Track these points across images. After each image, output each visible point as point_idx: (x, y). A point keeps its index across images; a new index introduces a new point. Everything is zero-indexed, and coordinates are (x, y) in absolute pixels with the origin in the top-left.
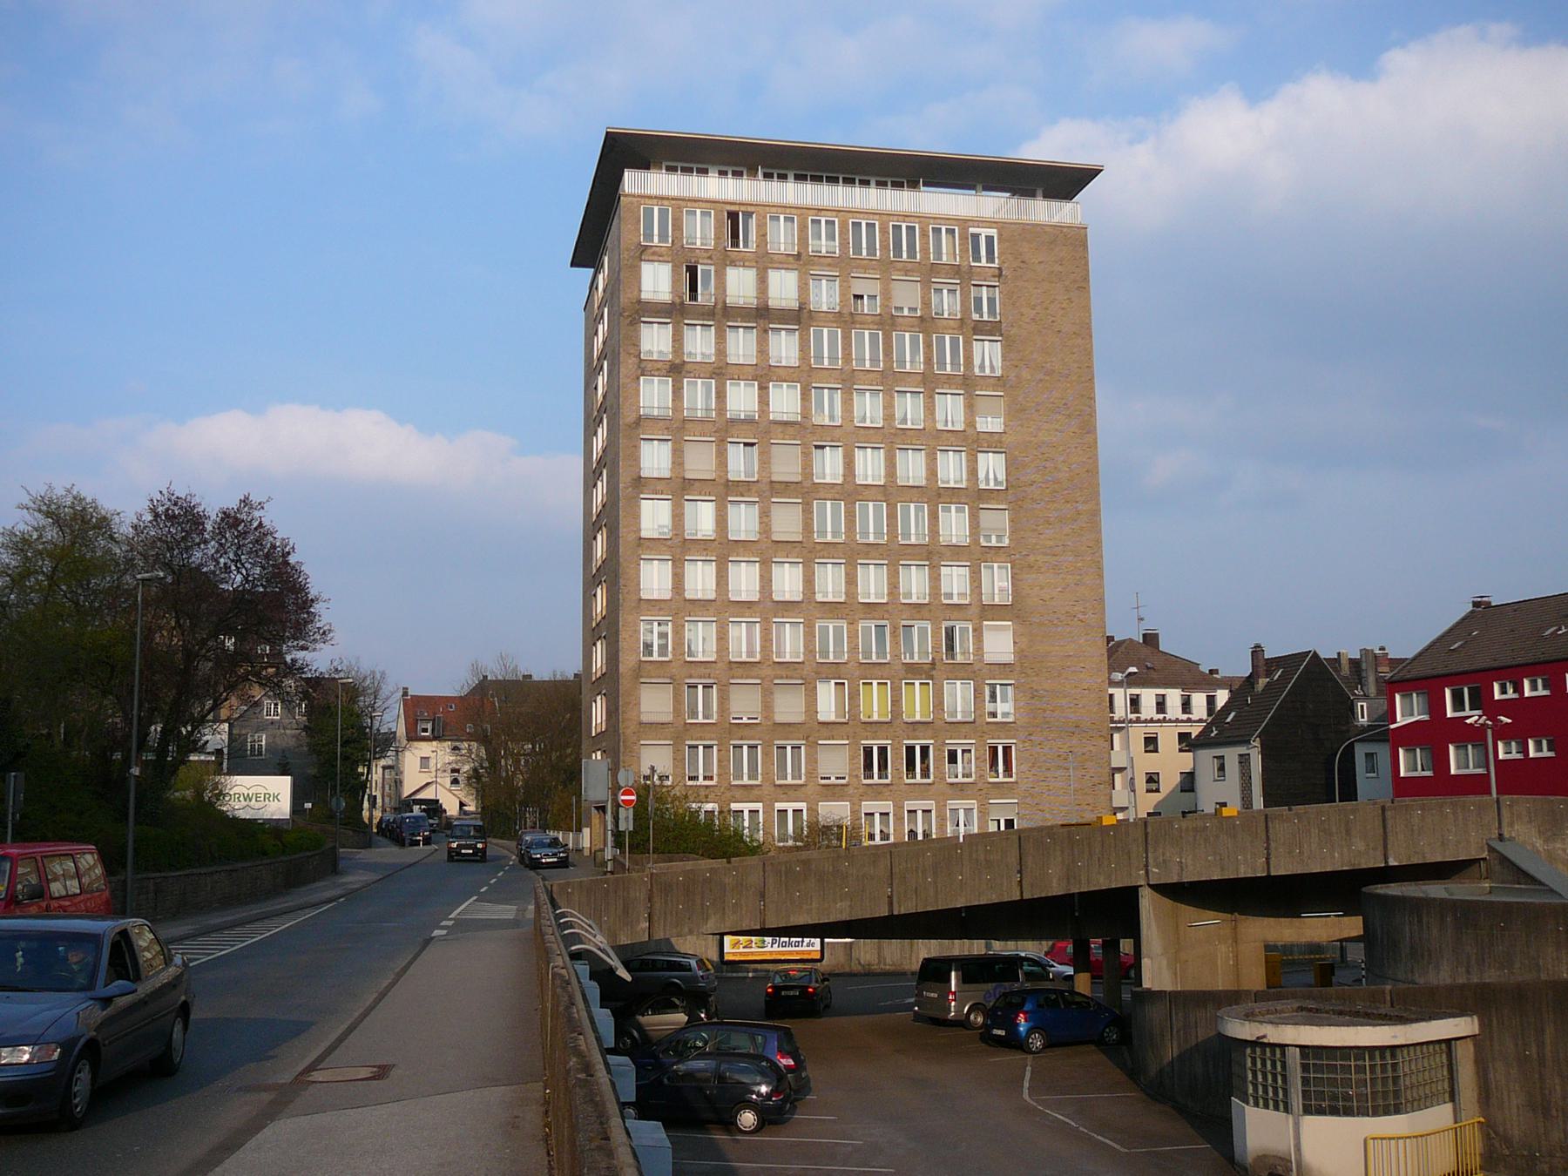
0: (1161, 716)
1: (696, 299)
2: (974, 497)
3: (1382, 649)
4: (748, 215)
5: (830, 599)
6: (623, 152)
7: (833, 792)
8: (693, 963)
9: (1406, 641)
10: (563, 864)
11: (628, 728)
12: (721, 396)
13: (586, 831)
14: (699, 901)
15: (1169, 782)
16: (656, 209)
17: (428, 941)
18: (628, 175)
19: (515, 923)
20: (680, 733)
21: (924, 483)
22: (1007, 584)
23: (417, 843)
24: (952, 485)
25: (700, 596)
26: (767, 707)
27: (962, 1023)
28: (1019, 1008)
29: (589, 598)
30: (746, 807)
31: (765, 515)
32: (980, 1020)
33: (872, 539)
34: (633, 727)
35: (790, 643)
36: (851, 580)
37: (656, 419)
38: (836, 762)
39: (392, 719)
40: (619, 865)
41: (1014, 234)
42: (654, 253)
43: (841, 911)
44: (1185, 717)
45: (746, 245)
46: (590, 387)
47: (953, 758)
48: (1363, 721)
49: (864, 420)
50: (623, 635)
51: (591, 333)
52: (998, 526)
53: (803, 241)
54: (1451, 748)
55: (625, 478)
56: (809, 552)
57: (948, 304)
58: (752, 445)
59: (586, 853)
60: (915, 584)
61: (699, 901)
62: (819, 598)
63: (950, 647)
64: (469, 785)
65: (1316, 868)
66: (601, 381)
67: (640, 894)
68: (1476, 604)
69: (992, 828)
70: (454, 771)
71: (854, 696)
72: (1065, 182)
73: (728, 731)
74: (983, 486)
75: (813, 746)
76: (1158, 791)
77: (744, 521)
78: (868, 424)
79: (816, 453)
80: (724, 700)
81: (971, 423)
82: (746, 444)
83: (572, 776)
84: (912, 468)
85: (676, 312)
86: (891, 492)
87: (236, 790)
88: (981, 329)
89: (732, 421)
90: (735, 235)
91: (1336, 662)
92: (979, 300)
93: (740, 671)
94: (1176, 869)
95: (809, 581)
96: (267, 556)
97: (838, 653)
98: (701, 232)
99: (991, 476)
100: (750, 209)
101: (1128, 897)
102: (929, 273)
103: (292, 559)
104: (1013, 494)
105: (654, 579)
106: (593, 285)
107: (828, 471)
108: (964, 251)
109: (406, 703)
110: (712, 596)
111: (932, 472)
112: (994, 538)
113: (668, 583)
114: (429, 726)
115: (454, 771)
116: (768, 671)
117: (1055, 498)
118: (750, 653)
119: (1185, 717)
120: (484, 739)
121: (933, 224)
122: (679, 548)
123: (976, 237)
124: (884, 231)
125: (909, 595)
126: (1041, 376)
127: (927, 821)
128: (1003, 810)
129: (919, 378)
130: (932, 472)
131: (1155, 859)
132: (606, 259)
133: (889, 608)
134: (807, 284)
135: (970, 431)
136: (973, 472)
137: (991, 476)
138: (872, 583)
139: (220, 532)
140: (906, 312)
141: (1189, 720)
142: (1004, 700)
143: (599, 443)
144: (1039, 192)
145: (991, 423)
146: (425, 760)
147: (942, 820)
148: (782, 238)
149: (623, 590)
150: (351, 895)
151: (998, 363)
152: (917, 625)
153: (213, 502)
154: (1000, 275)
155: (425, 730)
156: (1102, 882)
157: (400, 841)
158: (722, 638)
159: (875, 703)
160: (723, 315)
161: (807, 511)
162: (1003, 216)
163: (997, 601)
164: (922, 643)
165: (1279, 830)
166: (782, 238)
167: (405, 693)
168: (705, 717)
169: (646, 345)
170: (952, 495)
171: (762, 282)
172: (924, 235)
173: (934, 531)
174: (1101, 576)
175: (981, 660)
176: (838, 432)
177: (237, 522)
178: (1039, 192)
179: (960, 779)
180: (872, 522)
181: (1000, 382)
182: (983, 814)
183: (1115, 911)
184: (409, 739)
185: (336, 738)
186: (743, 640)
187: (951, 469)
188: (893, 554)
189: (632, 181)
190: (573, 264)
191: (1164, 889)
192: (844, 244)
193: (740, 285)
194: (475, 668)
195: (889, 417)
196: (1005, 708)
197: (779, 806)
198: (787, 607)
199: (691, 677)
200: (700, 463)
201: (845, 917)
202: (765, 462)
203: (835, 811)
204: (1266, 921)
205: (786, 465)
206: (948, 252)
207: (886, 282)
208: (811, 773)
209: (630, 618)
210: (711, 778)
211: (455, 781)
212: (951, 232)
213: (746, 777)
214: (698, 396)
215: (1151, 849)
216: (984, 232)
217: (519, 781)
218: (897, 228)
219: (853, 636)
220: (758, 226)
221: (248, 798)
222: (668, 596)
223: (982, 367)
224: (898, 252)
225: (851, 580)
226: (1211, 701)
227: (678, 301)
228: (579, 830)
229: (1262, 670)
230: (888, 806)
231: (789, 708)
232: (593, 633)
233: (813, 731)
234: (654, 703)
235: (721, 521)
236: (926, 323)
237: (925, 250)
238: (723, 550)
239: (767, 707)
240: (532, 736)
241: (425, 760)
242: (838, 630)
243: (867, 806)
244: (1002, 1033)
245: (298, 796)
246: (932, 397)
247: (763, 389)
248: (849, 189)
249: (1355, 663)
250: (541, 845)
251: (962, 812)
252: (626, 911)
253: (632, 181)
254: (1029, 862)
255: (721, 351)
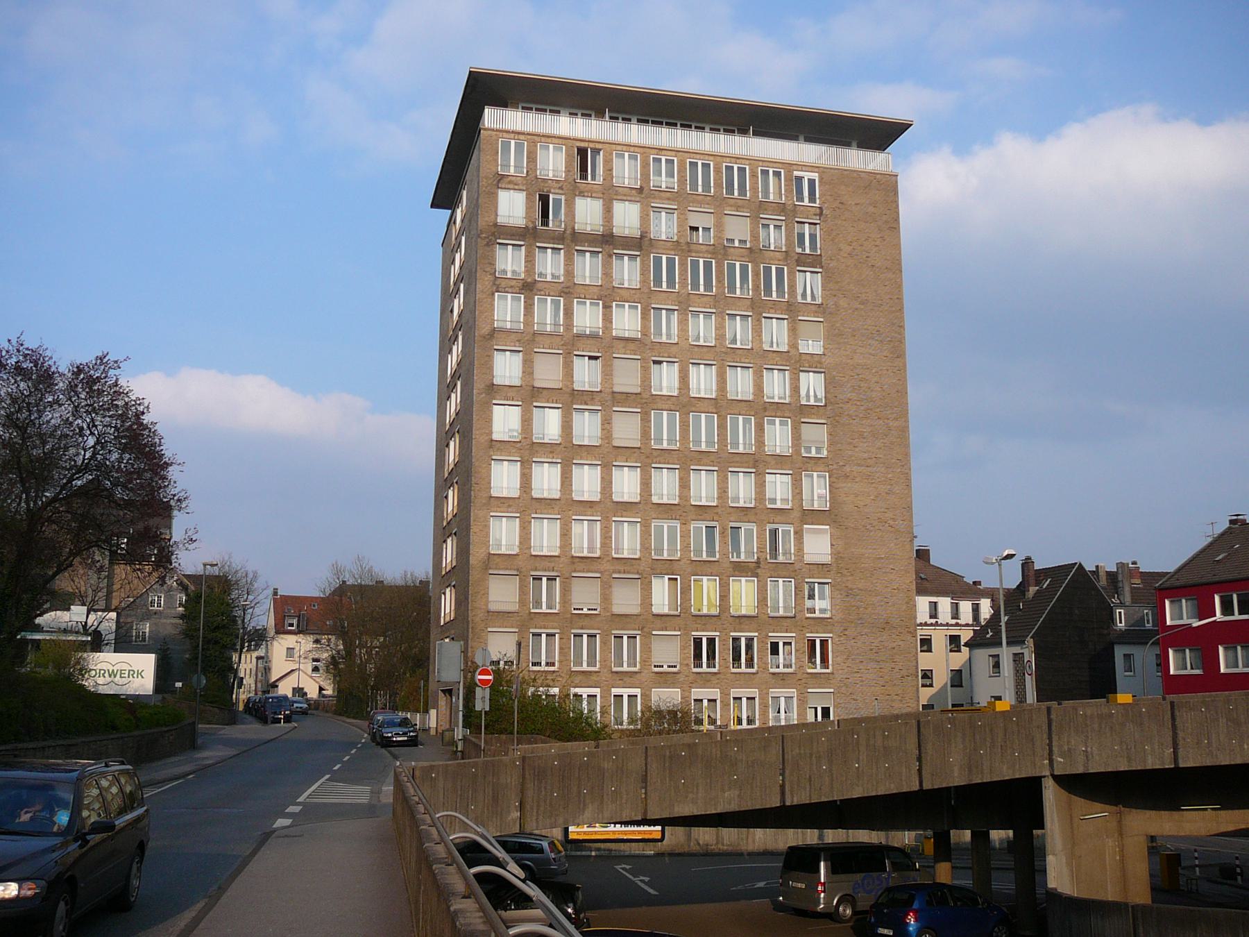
0: (933, 621)
1: (547, 225)
2: (796, 412)
3: (1134, 563)
4: (596, 152)
5: (665, 501)
6: (484, 90)
7: (665, 679)
8: (545, 844)
9: (1166, 555)
10: (413, 742)
11: (476, 616)
12: (569, 313)
13: (433, 712)
14: (575, 789)
15: (941, 678)
16: (513, 142)
17: (267, 836)
18: (488, 111)
19: (370, 810)
20: (525, 622)
21: (751, 398)
22: (825, 492)
23: (278, 721)
24: (776, 400)
25: (546, 495)
26: (606, 598)
27: (831, 916)
28: (906, 906)
29: (440, 499)
30: (584, 692)
31: (607, 422)
32: (849, 912)
33: (703, 447)
34: (481, 615)
35: (628, 541)
36: (684, 485)
37: (509, 332)
38: (668, 651)
39: (262, 616)
40: (471, 748)
41: (834, 178)
42: (510, 182)
43: (728, 802)
44: (954, 622)
45: (593, 178)
46: (446, 309)
47: (775, 649)
48: (1121, 625)
49: (698, 338)
50: (474, 529)
51: (448, 261)
52: (817, 437)
53: (645, 176)
54: (1221, 649)
55: (479, 385)
56: (646, 457)
57: (774, 238)
58: (596, 358)
59: (433, 732)
60: (742, 489)
61: (575, 789)
62: (655, 499)
63: (774, 548)
64: (328, 671)
65: (1225, 760)
66: (458, 305)
67: (511, 779)
68: (1231, 522)
69: (810, 718)
70: (314, 660)
71: (686, 590)
72: (879, 134)
73: (570, 620)
74: (804, 402)
75: (647, 636)
76: (931, 685)
77: (587, 428)
78: (701, 343)
79: (655, 369)
80: (566, 591)
81: (793, 345)
82: (591, 358)
83: (422, 662)
84: (741, 384)
85: (527, 236)
86: (721, 405)
87: (99, 667)
88: (804, 261)
89: (579, 336)
90: (583, 169)
91: (1096, 573)
92: (801, 237)
93: (581, 566)
94: (1081, 759)
95: (646, 484)
96: (123, 417)
97: (672, 550)
98: (554, 164)
99: (812, 393)
100: (598, 146)
101: (1032, 786)
102: (758, 210)
103: (146, 419)
104: (830, 410)
105: (503, 478)
106: (452, 220)
107: (664, 384)
108: (788, 191)
109: (275, 601)
110: (557, 495)
111: (759, 387)
112: (813, 450)
113: (517, 483)
114: (295, 622)
115: (314, 660)
116: (606, 566)
117: (866, 420)
118: (591, 549)
119: (954, 622)
120: (342, 633)
121: (763, 167)
122: (528, 450)
123: (800, 179)
124: (718, 171)
125: (737, 499)
126: (857, 305)
127: (751, 708)
128: (821, 696)
129: (749, 303)
130: (759, 387)
131: (1060, 747)
132: (465, 193)
133: (719, 510)
134: (648, 215)
135: (793, 352)
136: (795, 389)
137: (812, 393)
138: (704, 488)
139: (72, 388)
140: (737, 244)
141: (957, 625)
142: (822, 597)
143: (453, 360)
144: (854, 144)
145: (811, 346)
146: (290, 650)
147: (764, 707)
148: (626, 172)
149: (475, 487)
150: (202, 771)
151: (819, 292)
152: (744, 527)
153: (64, 356)
154: (821, 214)
155: (292, 625)
156: (1005, 772)
157: (264, 720)
158: (566, 534)
159: (706, 594)
160: (572, 240)
161: (645, 420)
162: (823, 162)
163: (816, 507)
164: (749, 544)
165: (1187, 719)
166: (626, 172)
167: (275, 593)
168: (548, 607)
169: (499, 266)
170: (777, 409)
171: (608, 211)
172: (754, 175)
173: (760, 442)
174: (909, 486)
175: (802, 560)
176: (674, 349)
177: (91, 381)
178: (854, 144)
179: (781, 669)
180: (704, 431)
181: (820, 309)
182: (802, 702)
183: (1018, 802)
184: (278, 632)
185: (210, 628)
186: (585, 538)
187: (776, 386)
188: (724, 462)
189: (492, 117)
190: (432, 206)
191: (1076, 784)
192: (682, 181)
193: (587, 213)
194: (338, 572)
195: (720, 337)
196: (821, 604)
197: (615, 691)
198: (625, 507)
199: (536, 570)
200: (548, 373)
201: (733, 807)
202: (607, 374)
203: (667, 697)
204: (1149, 813)
205: (627, 378)
206: (774, 191)
207: (719, 216)
208: (645, 661)
209: (481, 513)
210: (553, 664)
211: (316, 669)
212: (777, 174)
213: (585, 664)
214: (547, 314)
215: (1055, 738)
216: (807, 176)
217: (371, 667)
218: (730, 169)
219: (685, 535)
220: (605, 161)
221: (112, 674)
222: (516, 494)
223: (804, 295)
224: (730, 189)
225: (684, 485)
226: (976, 610)
227: (531, 226)
228: (426, 711)
229: (1032, 580)
230: (715, 693)
231: (625, 600)
232: (443, 532)
233: (648, 622)
234: (501, 594)
235: (567, 426)
236: (755, 253)
237: (754, 189)
238: (568, 453)
239: (606, 598)
240: (384, 635)
241: (290, 650)
242: (672, 530)
243: (696, 693)
244: (889, 932)
245: (163, 674)
246: (759, 320)
247: (607, 307)
248: (686, 132)
249: (1112, 576)
250: (391, 724)
251: (782, 700)
252: (495, 799)
253: (492, 117)
254: (929, 749)
255: (569, 273)
